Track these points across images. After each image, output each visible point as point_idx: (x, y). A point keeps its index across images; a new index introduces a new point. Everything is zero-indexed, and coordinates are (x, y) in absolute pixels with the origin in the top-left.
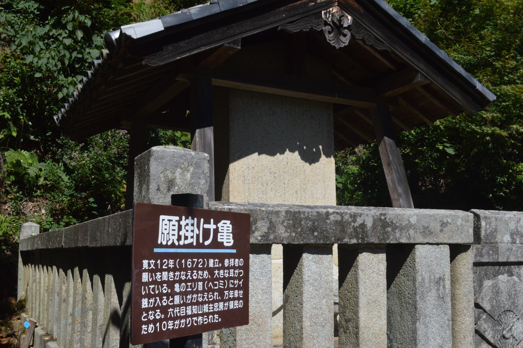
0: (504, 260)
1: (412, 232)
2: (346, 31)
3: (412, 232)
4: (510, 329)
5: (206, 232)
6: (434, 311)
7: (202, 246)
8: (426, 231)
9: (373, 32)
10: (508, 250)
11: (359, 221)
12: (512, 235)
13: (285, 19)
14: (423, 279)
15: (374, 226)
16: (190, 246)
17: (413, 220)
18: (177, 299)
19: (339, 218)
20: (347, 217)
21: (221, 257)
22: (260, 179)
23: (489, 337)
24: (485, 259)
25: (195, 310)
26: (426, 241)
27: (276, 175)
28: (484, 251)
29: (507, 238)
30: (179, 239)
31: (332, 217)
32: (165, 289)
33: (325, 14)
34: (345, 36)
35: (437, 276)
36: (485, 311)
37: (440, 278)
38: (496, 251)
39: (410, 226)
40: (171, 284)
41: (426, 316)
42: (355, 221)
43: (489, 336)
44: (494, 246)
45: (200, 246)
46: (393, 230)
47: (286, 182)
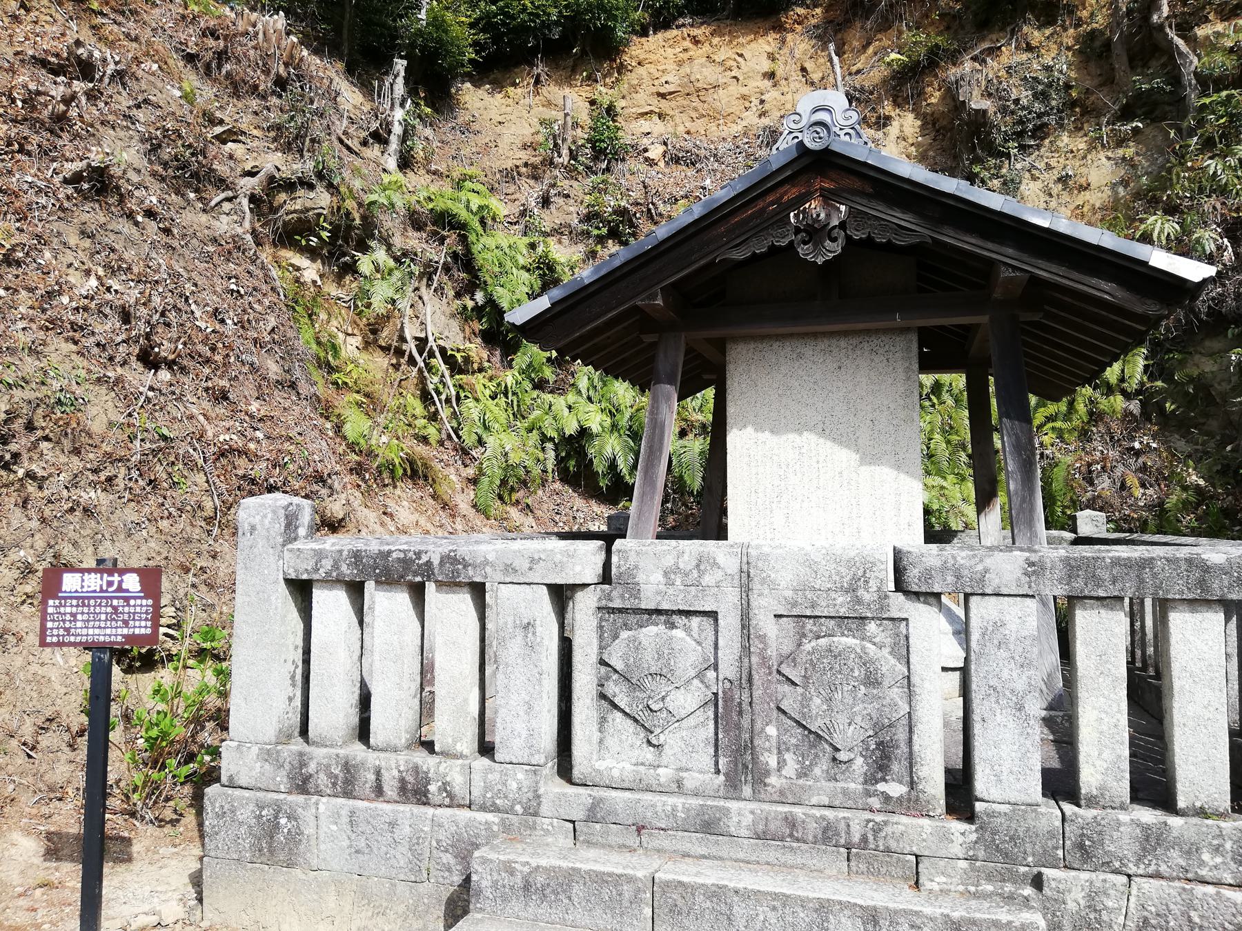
0: (652, 606)
1: (488, 569)
2: (835, 233)
3: (488, 569)
4: (663, 699)
5: (110, 584)
6: (519, 661)
7: (106, 591)
8: (509, 568)
9: (888, 218)
10: (658, 593)
11: (424, 559)
12: (666, 574)
13: (727, 243)
14: (506, 623)
15: (442, 563)
16: (95, 591)
17: (491, 557)
18: (79, 624)
19: (402, 555)
20: (411, 555)
21: (127, 599)
22: (775, 458)
23: (622, 705)
24: (617, 604)
25: (97, 631)
26: (508, 580)
27: (803, 450)
28: (615, 594)
29: (658, 577)
30: (82, 587)
31: (394, 555)
32: (68, 617)
33: (796, 216)
34: (834, 240)
35: (526, 621)
36: (616, 671)
37: (529, 624)
38: (636, 594)
39: (486, 562)
40: (74, 615)
41: (507, 665)
42: (419, 558)
43: (622, 701)
44: (634, 589)
45: (102, 591)
46: (465, 567)
47: (821, 459)
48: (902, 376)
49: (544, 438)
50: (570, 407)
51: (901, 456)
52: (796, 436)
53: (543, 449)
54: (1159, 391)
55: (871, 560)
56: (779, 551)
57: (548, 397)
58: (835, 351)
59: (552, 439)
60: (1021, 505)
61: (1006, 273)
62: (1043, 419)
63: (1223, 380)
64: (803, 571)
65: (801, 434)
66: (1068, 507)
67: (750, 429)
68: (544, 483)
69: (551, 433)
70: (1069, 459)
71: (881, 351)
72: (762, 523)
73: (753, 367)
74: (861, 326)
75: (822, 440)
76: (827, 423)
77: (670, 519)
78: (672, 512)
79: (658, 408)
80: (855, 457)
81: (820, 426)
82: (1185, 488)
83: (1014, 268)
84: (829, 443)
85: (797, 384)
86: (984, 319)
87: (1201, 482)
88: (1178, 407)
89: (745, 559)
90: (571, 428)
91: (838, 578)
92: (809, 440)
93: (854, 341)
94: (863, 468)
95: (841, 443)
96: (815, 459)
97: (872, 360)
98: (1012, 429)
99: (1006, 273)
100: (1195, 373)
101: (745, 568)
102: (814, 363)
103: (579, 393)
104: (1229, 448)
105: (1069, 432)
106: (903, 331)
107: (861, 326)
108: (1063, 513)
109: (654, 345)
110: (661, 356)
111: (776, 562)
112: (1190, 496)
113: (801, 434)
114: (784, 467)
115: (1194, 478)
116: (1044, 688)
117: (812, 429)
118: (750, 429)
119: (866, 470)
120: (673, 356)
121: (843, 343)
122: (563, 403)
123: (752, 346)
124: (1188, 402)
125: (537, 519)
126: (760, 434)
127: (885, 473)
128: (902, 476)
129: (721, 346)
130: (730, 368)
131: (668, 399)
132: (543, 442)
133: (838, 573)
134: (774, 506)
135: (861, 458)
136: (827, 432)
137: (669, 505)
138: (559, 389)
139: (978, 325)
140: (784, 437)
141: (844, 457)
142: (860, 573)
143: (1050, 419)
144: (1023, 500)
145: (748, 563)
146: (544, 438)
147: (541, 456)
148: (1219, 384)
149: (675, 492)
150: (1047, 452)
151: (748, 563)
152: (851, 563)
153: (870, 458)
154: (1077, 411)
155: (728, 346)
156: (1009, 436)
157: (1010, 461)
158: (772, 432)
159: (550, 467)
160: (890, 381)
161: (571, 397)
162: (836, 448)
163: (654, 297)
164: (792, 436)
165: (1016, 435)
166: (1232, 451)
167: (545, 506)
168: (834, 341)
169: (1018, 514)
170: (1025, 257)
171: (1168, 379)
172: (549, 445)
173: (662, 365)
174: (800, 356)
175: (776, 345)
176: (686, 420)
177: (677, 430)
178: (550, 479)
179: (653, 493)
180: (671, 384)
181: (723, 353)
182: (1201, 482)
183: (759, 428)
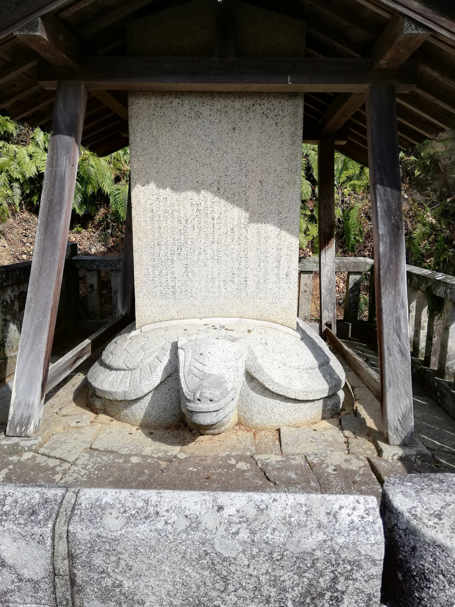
22: (175, 214)
47: (216, 216)
48: (288, 140)
49: (11, 180)
50: (31, 156)
51: (284, 215)
52: (194, 194)
53: (11, 187)
54: (411, 164)
55: (351, 556)
56: (144, 529)
57: (13, 147)
58: (231, 112)
59: (17, 180)
60: (388, 266)
61: (409, 30)
62: (346, 178)
63: (447, 158)
64: (194, 575)
65: (198, 192)
66: (358, 236)
67: (152, 186)
68: (14, 213)
69: (16, 175)
70: (359, 205)
71: (271, 115)
72: (164, 272)
73: (154, 123)
74: (256, 87)
75: (217, 199)
76: (222, 182)
77: (111, 240)
78: (112, 236)
79: (57, 160)
80: (245, 215)
81: (216, 185)
82: (424, 225)
83: (419, 25)
84: (223, 202)
85: (195, 143)
86: (358, 89)
87: (434, 221)
88: (421, 173)
89: (62, 548)
90: (31, 171)
91: (273, 592)
92: (206, 198)
93: (248, 103)
94: (251, 225)
95: (233, 202)
96: (210, 216)
97: (263, 124)
98: (385, 195)
99: (409, 30)
100: (432, 152)
101: (63, 566)
102: (211, 123)
103: (37, 145)
104: (449, 200)
105: (360, 186)
106: (292, 95)
107: (256, 87)
108: (355, 238)
109: (53, 94)
110: (60, 104)
111: (135, 554)
112: (426, 229)
113: (198, 192)
114: (184, 222)
115: (431, 220)
116: (399, 427)
117: (208, 188)
118: (152, 186)
119: (253, 227)
120: (73, 105)
121: (237, 104)
122: (25, 152)
123: (153, 101)
124: (425, 169)
125: (9, 241)
126: (161, 191)
127: (270, 229)
128: (284, 233)
129: (123, 98)
130: (132, 123)
131: (68, 151)
132: (11, 182)
133: (275, 582)
134: (175, 258)
135: (250, 217)
136: (222, 190)
137: (110, 231)
138: (24, 143)
139: (346, 96)
140: (183, 195)
141: (236, 214)
142: (324, 582)
143: (349, 179)
144: (390, 262)
145: (71, 556)
146: (11, 180)
147: (9, 192)
148: (444, 160)
149: (113, 221)
150: (346, 199)
151: (71, 556)
152: (303, 562)
153: (257, 217)
154: (365, 174)
155: (131, 100)
156: (382, 202)
157: (381, 226)
158: (173, 189)
159: (17, 202)
160: (278, 145)
161: (31, 148)
162: (229, 206)
163: (34, 27)
164: (190, 194)
165: (387, 200)
166: (450, 201)
167: (15, 231)
168: (229, 102)
169: (385, 274)
170: (430, 13)
171: (417, 155)
172: (16, 185)
173: (62, 116)
174: (198, 115)
175: (176, 102)
176: (120, 170)
177: (113, 177)
178: (18, 210)
179: (54, 248)
180: (70, 134)
181: (126, 105)
182: (434, 221)
183: (161, 185)
